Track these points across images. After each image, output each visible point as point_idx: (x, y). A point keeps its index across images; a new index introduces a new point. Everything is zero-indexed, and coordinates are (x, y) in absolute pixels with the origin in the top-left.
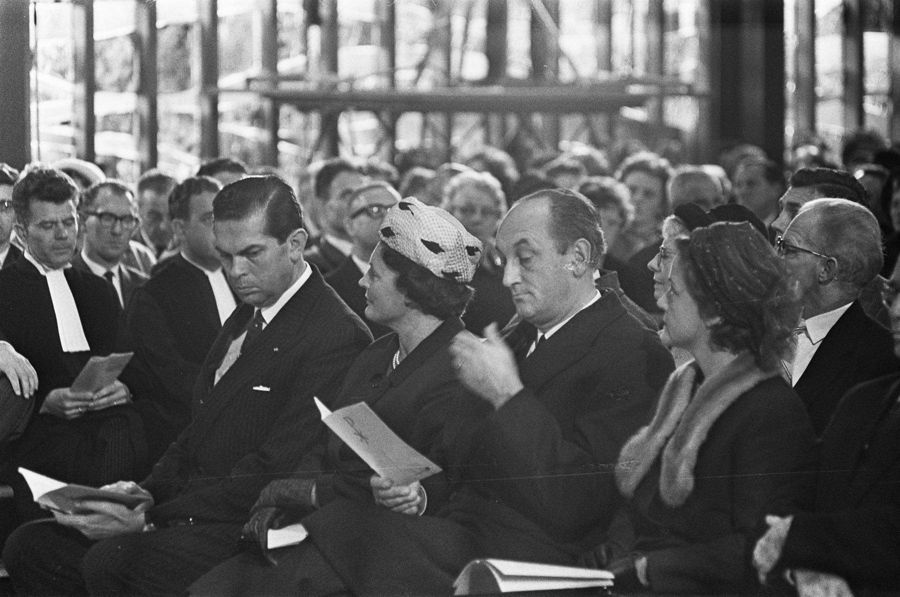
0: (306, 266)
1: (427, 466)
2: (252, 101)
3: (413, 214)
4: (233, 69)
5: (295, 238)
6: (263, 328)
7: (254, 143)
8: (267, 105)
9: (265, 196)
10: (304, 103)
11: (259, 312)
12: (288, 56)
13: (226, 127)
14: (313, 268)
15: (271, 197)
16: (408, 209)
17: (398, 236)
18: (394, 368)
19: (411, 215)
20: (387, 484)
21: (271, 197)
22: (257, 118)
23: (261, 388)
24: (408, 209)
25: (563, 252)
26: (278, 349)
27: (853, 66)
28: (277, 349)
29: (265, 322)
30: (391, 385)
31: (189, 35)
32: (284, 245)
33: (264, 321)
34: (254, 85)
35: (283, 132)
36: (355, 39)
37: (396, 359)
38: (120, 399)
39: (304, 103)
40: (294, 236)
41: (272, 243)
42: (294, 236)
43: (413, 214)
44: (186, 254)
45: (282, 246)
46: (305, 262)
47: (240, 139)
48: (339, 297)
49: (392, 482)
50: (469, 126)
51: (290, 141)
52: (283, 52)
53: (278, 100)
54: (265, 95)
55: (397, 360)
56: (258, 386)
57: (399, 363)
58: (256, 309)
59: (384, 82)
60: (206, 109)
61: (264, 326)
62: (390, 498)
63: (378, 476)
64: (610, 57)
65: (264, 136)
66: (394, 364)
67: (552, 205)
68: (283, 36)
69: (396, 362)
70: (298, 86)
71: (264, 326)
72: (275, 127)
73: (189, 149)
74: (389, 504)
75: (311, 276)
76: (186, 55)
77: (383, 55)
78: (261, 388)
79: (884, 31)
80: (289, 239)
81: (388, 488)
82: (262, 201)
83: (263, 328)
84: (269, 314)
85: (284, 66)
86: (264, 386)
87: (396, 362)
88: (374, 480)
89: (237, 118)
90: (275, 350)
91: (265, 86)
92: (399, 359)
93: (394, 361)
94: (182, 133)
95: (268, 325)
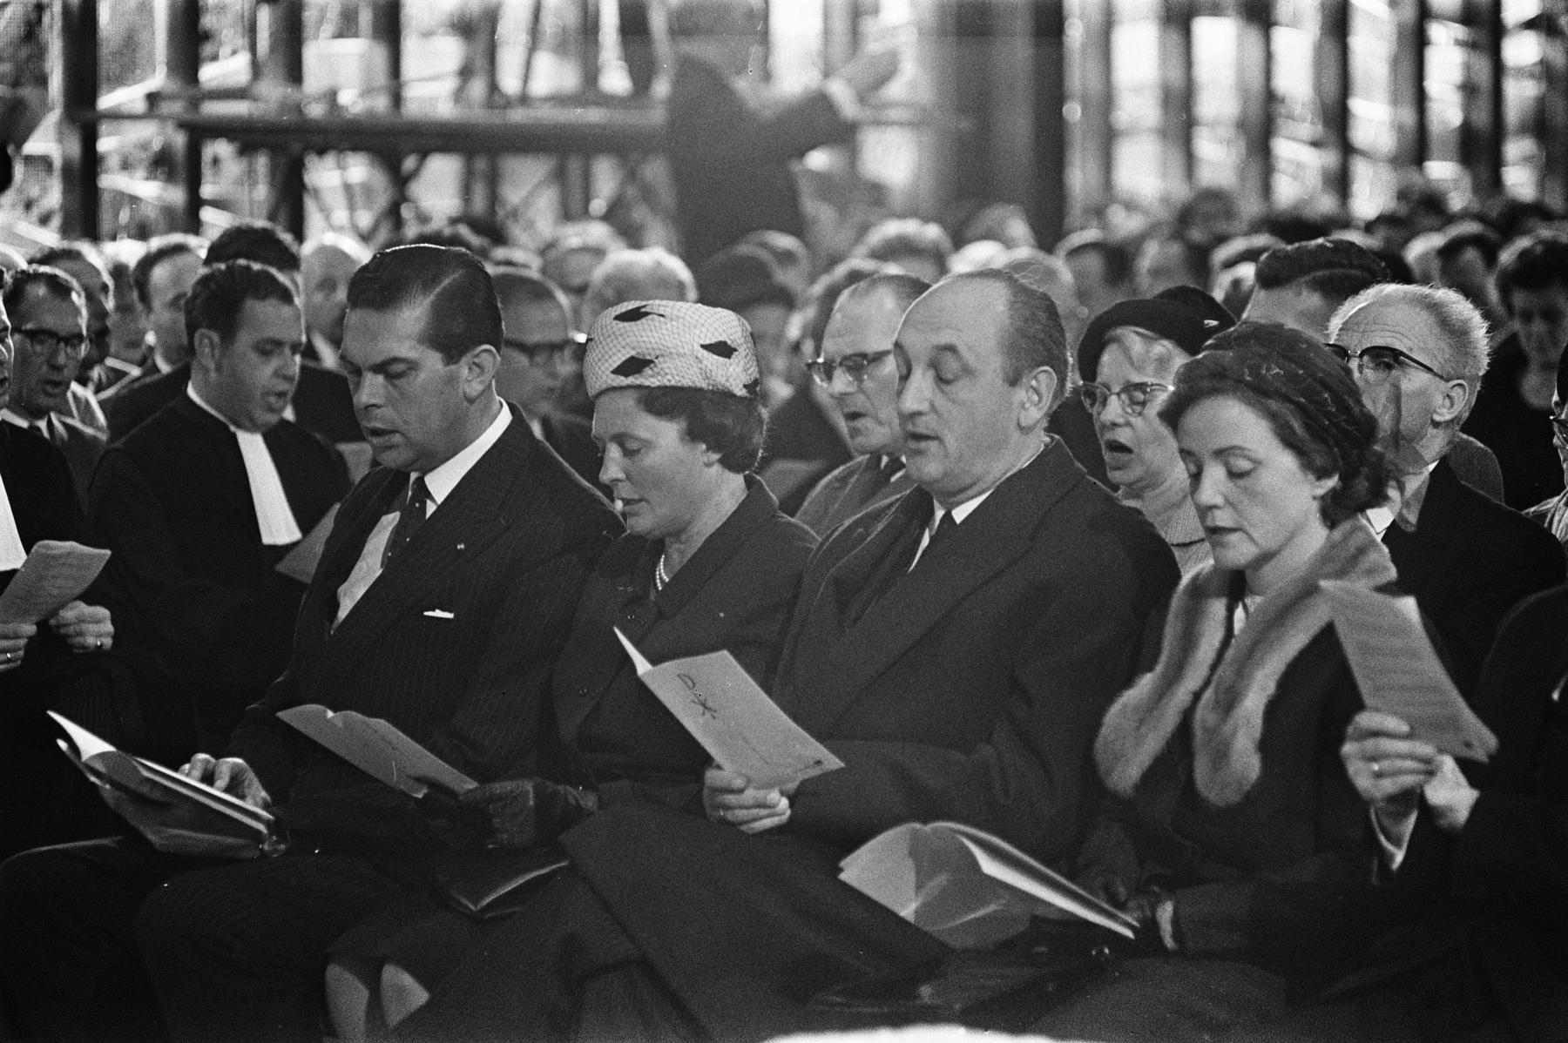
0: (501, 405)
1: (819, 756)
2: (150, 134)
3: (662, 316)
4: (119, 81)
5: (476, 360)
6: (429, 514)
7: (157, 206)
8: (179, 140)
9: (435, 280)
10: (247, 137)
11: (420, 482)
12: (215, 58)
13: (112, 180)
14: (512, 408)
15: (446, 282)
16: (647, 314)
17: (661, 359)
18: (660, 588)
19: (662, 319)
20: (739, 783)
21: (446, 282)
22: (162, 164)
23: (438, 613)
24: (647, 314)
25: (1013, 381)
26: (465, 545)
27: (1176, 76)
28: (462, 546)
29: (433, 500)
30: (660, 615)
31: (46, 19)
32: (453, 367)
33: (429, 495)
34: (167, 108)
35: (207, 190)
36: (328, 28)
37: (660, 575)
38: (99, 636)
39: (247, 137)
40: (477, 356)
41: (433, 362)
42: (477, 356)
43: (662, 316)
44: (198, 392)
45: (449, 368)
46: (498, 398)
47: (134, 199)
48: (561, 459)
49: (749, 781)
50: (535, 180)
51: (218, 204)
52: (207, 49)
53: (199, 132)
54: (182, 125)
55: (663, 574)
56: (434, 610)
57: (667, 580)
58: (413, 476)
59: (381, 103)
60: (75, 148)
61: (431, 509)
62: (741, 807)
63: (719, 767)
64: (766, 61)
65: (177, 196)
66: (658, 581)
67: (1012, 299)
68: (207, 21)
69: (661, 578)
70: (238, 108)
71: (431, 509)
72: (194, 183)
73: (44, 220)
74: (737, 817)
75: (509, 427)
76: (40, 53)
77: (380, 54)
78: (438, 613)
79: (1230, 16)
80: (465, 360)
81: (741, 791)
82: (427, 287)
83: (429, 514)
84: (442, 483)
85: (210, 74)
86: (443, 610)
87: (661, 578)
88: (711, 776)
89: (126, 166)
90: (459, 547)
91: (175, 108)
92: (665, 572)
93: (658, 577)
94: (34, 191)
95: (440, 508)
